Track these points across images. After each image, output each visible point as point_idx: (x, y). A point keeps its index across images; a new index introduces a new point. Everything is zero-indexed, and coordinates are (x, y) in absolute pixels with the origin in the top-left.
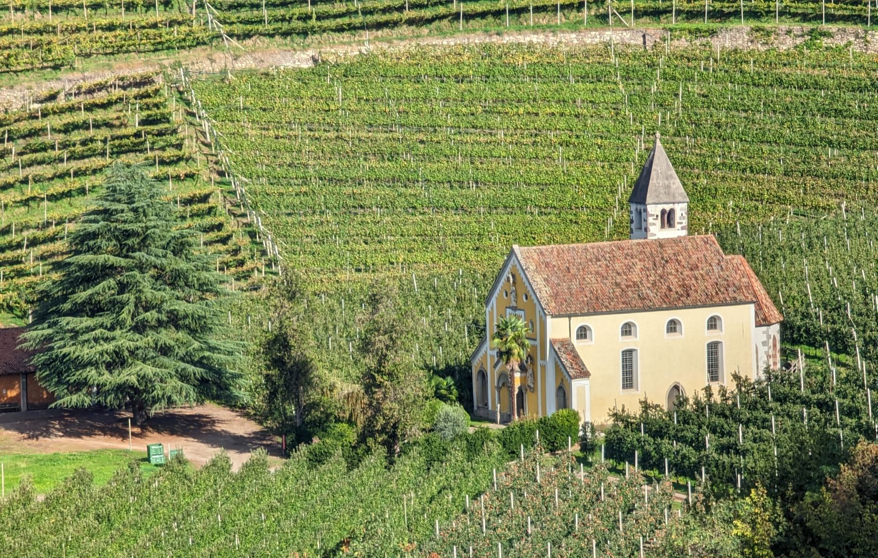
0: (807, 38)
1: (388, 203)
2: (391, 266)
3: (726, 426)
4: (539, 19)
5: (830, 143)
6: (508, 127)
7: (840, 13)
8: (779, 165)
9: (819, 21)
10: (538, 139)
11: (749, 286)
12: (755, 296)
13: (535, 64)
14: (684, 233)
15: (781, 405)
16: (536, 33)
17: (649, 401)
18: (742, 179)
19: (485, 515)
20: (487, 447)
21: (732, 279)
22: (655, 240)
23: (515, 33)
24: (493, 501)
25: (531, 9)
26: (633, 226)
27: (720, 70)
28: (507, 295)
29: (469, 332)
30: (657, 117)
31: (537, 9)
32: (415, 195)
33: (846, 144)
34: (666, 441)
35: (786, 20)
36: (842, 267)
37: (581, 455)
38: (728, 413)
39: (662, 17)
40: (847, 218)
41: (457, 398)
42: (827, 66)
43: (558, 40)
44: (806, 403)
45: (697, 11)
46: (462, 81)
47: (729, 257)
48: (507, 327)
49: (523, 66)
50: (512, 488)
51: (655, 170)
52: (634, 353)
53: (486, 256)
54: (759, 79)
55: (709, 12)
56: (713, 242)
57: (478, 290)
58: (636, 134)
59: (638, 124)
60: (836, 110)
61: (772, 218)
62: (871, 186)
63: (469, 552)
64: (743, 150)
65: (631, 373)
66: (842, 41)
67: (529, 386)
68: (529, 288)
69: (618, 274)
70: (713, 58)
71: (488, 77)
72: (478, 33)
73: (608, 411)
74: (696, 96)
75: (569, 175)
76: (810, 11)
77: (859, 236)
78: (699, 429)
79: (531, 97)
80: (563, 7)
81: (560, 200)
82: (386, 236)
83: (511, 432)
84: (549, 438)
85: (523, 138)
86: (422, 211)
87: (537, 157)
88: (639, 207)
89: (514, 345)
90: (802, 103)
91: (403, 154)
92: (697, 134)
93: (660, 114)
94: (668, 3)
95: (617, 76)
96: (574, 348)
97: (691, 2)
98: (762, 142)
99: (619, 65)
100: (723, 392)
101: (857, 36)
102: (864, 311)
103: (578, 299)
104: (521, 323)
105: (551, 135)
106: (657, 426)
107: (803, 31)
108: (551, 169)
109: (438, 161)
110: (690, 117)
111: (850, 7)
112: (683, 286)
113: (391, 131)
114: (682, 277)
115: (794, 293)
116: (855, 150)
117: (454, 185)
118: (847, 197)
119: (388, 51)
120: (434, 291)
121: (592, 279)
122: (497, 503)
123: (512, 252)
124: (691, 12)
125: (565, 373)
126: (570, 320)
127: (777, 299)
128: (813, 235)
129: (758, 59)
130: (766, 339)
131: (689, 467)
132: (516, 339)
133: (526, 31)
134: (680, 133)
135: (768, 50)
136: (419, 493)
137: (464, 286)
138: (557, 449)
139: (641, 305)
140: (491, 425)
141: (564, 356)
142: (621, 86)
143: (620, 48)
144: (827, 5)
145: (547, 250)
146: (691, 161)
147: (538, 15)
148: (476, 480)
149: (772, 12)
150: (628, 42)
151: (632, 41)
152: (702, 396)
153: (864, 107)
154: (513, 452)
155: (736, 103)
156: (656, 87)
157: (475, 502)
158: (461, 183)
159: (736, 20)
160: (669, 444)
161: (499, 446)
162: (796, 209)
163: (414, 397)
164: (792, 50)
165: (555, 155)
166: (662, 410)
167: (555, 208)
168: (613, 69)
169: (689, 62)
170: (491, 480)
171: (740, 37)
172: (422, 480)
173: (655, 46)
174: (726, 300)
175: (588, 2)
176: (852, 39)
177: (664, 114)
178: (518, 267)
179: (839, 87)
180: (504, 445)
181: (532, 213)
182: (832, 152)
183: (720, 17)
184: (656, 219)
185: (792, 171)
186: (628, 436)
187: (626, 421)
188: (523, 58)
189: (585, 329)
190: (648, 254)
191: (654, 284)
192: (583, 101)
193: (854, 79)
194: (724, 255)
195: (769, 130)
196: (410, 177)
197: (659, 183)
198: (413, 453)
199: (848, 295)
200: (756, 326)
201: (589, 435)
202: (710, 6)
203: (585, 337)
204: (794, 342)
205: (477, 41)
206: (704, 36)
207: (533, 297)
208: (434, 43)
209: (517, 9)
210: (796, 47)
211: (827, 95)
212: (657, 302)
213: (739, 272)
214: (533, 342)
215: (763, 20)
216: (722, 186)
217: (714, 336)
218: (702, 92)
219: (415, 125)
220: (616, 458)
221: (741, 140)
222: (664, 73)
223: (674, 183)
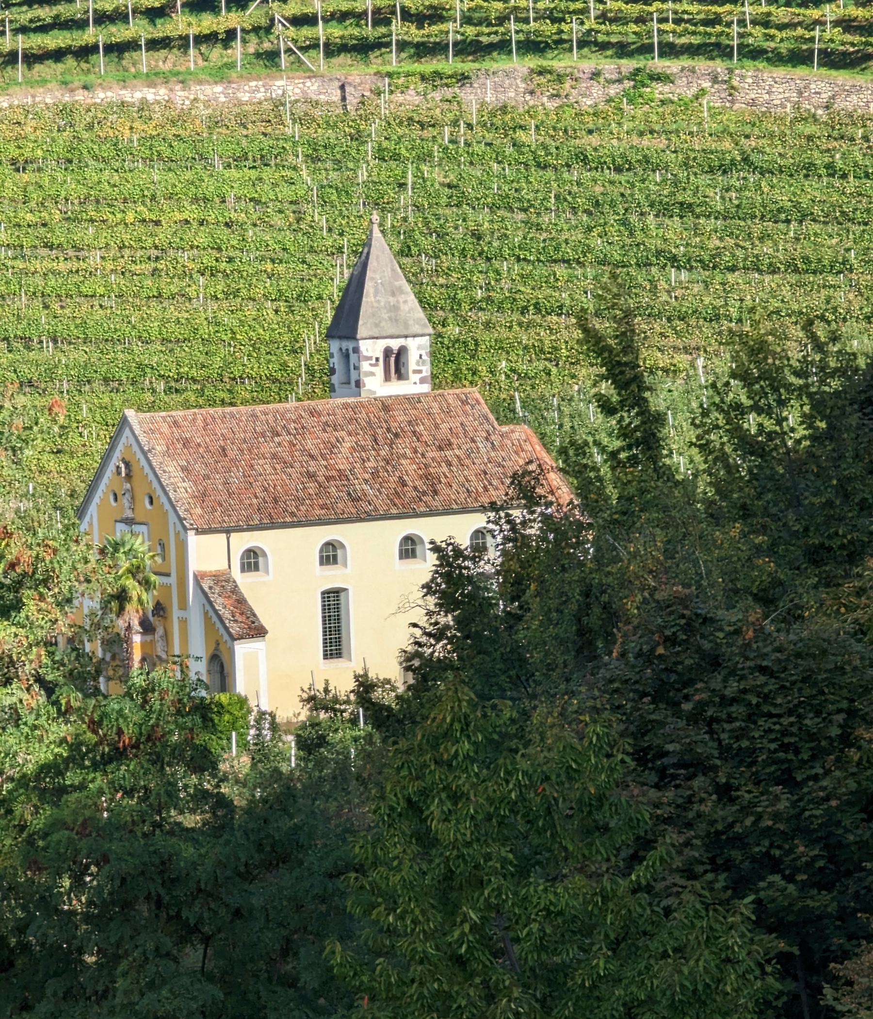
0: (628, 84)
4: (157, 61)
5: (674, 259)
6: (107, 244)
7: (684, 40)
8: (585, 300)
9: (647, 56)
13: (152, 137)
14: (426, 388)
16: (152, 85)
17: (372, 675)
18: (520, 324)
21: (510, 464)
23: (115, 86)
26: (335, 379)
27: (479, 142)
28: (116, 499)
33: (700, 261)
39: (372, 55)
43: (192, 97)
45: (435, 43)
46: (24, 169)
47: (505, 429)
49: (132, 141)
51: (372, 279)
52: (342, 595)
53: (73, 464)
55: (456, 44)
56: (477, 401)
60: (682, 204)
61: (576, 387)
64: (522, 276)
65: (338, 630)
67: (159, 657)
68: (155, 484)
69: (312, 457)
70: (465, 123)
71: (70, 161)
72: (49, 86)
73: (300, 693)
74: (437, 186)
76: (632, 38)
79: (146, 193)
85: (134, 262)
87: (160, 295)
90: (622, 195)
92: (440, 250)
94: (383, 30)
95: (297, 156)
96: (236, 586)
97: (423, 28)
98: (555, 261)
99: (300, 137)
101: (715, 80)
105: (184, 257)
107: (620, 73)
110: (427, 224)
112: (427, 477)
114: (424, 460)
118: (705, 351)
121: (266, 467)
123: (124, 421)
124: (423, 44)
125: (222, 631)
129: (542, 122)
132: (134, 572)
133: (135, 82)
134: (410, 250)
135: (561, 107)
139: (354, 511)
141: (220, 600)
142: (304, 173)
143: (301, 109)
145: (185, 418)
146: (431, 297)
147: (156, 54)
149: (565, 41)
150: (315, 98)
151: (322, 97)
155: (507, 196)
156: (365, 174)
158: (26, 341)
159: (504, 57)
165: (191, 291)
169: (423, 129)
171: (511, 85)
173: (363, 103)
175: (243, 30)
176: (706, 84)
177: (383, 219)
178: (135, 448)
181: (154, 391)
182: (676, 277)
183: (473, 53)
184: (376, 365)
188: (131, 128)
189: (255, 553)
190: (363, 423)
191: (375, 474)
193: (712, 152)
194: (496, 423)
195: (566, 242)
197: (378, 301)
202: (458, 32)
205: (49, 101)
206: (447, 86)
207: (164, 499)
209: (117, 44)
211: (664, 181)
212: (381, 504)
213: (522, 454)
214: (165, 580)
218: (447, 181)
221: (518, 259)
222: (380, 149)
223: (405, 302)
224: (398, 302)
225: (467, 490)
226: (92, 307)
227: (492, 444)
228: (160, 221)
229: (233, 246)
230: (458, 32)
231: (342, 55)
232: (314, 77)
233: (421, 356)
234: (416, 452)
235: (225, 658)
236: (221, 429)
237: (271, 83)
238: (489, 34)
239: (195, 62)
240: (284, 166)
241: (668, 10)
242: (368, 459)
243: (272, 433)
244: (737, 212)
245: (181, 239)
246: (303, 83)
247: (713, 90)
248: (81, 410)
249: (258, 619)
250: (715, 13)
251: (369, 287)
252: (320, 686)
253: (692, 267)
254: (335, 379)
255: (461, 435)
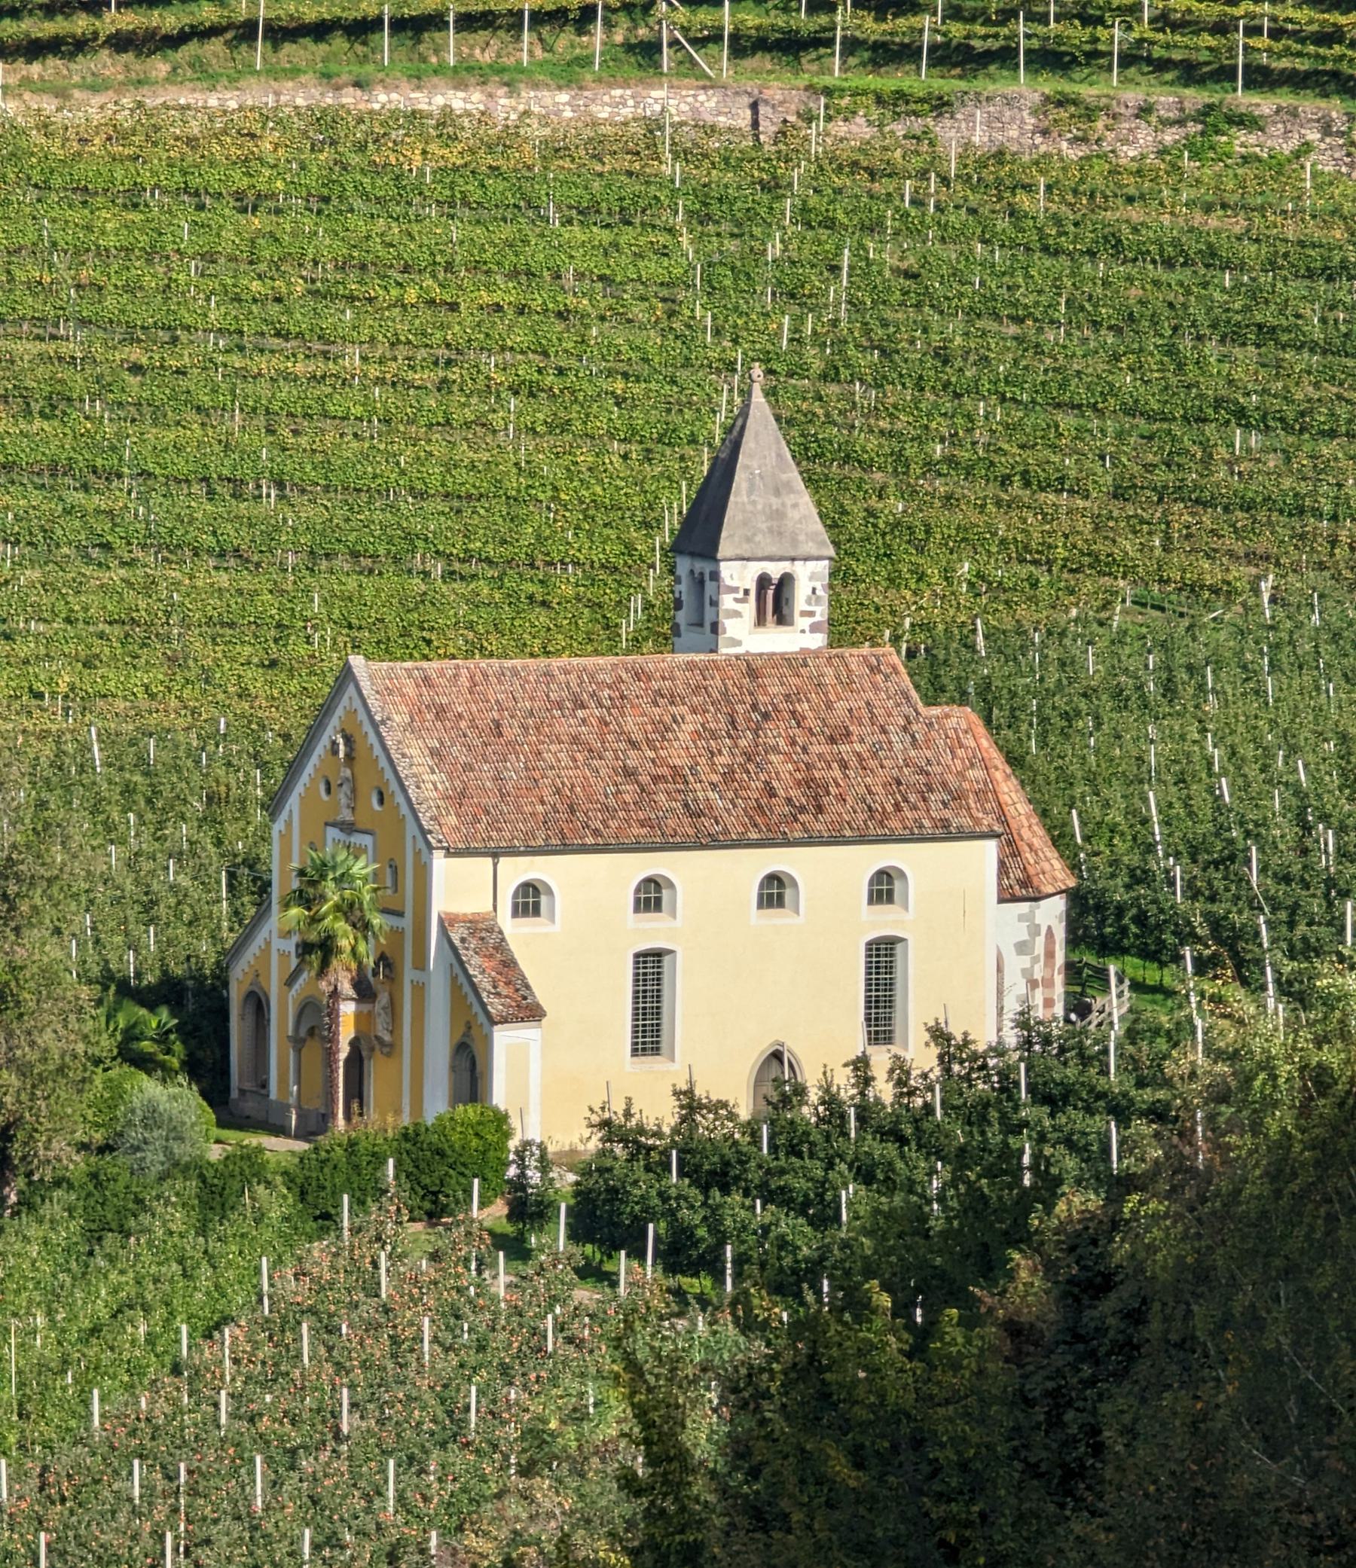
0: (1193, 128)
1: (36, 530)
2: (34, 702)
3: (900, 1165)
4: (472, 48)
5: (1241, 414)
6: (372, 339)
7: (1285, 63)
8: (1100, 471)
9: (1227, 85)
10: (454, 374)
11: (986, 792)
12: (1003, 818)
13: (456, 169)
14: (817, 641)
15: (1052, 1115)
16: (461, 85)
17: (699, 1092)
18: (998, 503)
19: (233, 1380)
20: (253, 1199)
21: (939, 769)
22: (737, 658)
23: (404, 85)
24: (256, 1345)
25: (451, 19)
26: (682, 617)
27: (957, 207)
28: (328, 791)
29: (231, 887)
30: (780, 326)
31: (469, 22)
32: (110, 513)
33: (1282, 420)
34: (737, 1197)
35: (1140, 78)
36: (1248, 751)
37: (509, 1229)
38: (908, 1130)
40: (1273, 618)
41: (183, 1063)
42: (1243, 207)
43: (521, 108)
44: (1121, 1111)
45: (902, 45)
46: (255, 208)
47: (936, 711)
48: (323, 877)
49: (424, 175)
50: (312, 1311)
51: (746, 467)
52: (666, 959)
53: (294, 686)
54: (1060, 234)
55: (933, 48)
57: (266, 776)
58: (718, 371)
59: (727, 344)
60: (1260, 326)
62: (1343, 536)
63: (178, 1477)
64: (1007, 426)
65: (657, 1013)
66: (1286, 140)
67: (377, 1038)
68: (389, 774)
69: (634, 744)
70: (938, 175)
71: (326, 200)
72: (303, 79)
73: (588, 1114)
75: (532, 475)
76: (1204, 56)
77: (1301, 667)
78: (826, 1170)
79: (438, 259)
80: (540, 18)
81: (504, 542)
82: (26, 621)
83: (324, 1162)
84: (426, 1180)
85: (411, 368)
86: (127, 557)
87: (448, 422)
88: (700, 566)
89: (341, 926)
90: (1171, 305)
91: (82, 400)
92: (884, 377)
93: (786, 320)
94: (823, 19)
96: (503, 940)
97: (884, 20)
98: (1058, 406)
99: (683, 181)
100: (900, 1073)
101: (1327, 130)
102: (1296, 869)
103: (519, 809)
104: (360, 868)
106: (716, 1159)
107: (1182, 110)
108: (485, 456)
109: (178, 423)
110: (867, 331)
111: (1311, 49)
113: (53, 337)
114: (805, 758)
115: (1115, 816)
116: (1307, 436)
117: (219, 489)
118: (1278, 564)
119: (58, 118)
120: (146, 774)
122: (267, 1350)
123: (346, 675)
125: (476, 1008)
126: (495, 865)
127: (1067, 830)
128: (1180, 659)
129: (1057, 182)
130: (1026, 937)
131: (795, 1272)
133: (435, 80)
134: (837, 373)
135: (1088, 158)
136: (59, 1317)
137: (229, 764)
138: (444, 1211)
139: (691, 831)
140: (269, 1142)
141: (476, 960)
142: (684, 240)
143: (686, 140)
144: (1251, 42)
145: (441, 673)
148: (217, 1286)
150: (710, 119)
151: (722, 119)
152: (844, 1083)
153: (1336, 321)
154: (326, 1216)
156: (779, 245)
157: (205, 1345)
158: (236, 484)
159: (1005, 73)
160: (743, 1206)
161: (285, 1197)
162: (1140, 590)
163: (62, 1057)
164: (1151, 160)
165: (497, 419)
166: (732, 1116)
167: (489, 561)
168: (667, 192)
169: (873, 181)
170: (257, 1286)
171: (1013, 119)
172: (68, 1280)
173: (784, 134)
174: (922, 826)
175: (606, 7)
176: (1313, 136)
178: (362, 716)
179: (1271, 265)
180: (303, 1195)
181: (426, 574)
182: (1244, 441)
185: (1134, 486)
186: (635, 1183)
187: (635, 1142)
188: (424, 152)
189: (535, 888)
190: (716, 694)
191: (729, 775)
192: (580, 276)
193: (1314, 246)
194: (920, 705)
196: (99, 462)
197: (754, 503)
198: (54, 1207)
199: (1257, 825)
200: (1001, 901)
201: (534, 1176)
202: (937, 31)
203: (536, 912)
204: (1108, 947)
205: (300, 102)
206: (915, 113)
207: (400, 799)
208: (182, 101)
209: (412, 18)
210: (1162, 152)
212: (734, 823)
213: (960, 752)
214: (394, 921)
215: (1076, 76)
216: (947, 521)
217: (883, 922)
218: (904, 265)
219: (119, 322)
220: (601, 1243)
221: (1003, 399)
222: (805, 209)
224: (783, 505)
225: (870, 808)
226: (341, 435)
227: (913, 736)
228: (457, 304)
229: (566, 351)
230: (937, 31)
231: (759, 55)
232: (712, 87)
233: (814, 590)
234: (793, 743)
235: (477, 1048)
236: (496, 692)
237: (644, 93)
238: (985, 37)
239: (531, 53)
240: (654, 227)
241: (1263, 15)
242: (720, 752)
243: (575, 703)
244: (1344, 344)
245: (487, 335)
246: (695, 96)
247: (1323, 146)
248: (312, 601)
249: (533, 994)
250: (1335, 25)
251: (740, 479)
252: (619, 1107)
253: (1267, 427)
254: (682, 617)
255: (866, 721)
